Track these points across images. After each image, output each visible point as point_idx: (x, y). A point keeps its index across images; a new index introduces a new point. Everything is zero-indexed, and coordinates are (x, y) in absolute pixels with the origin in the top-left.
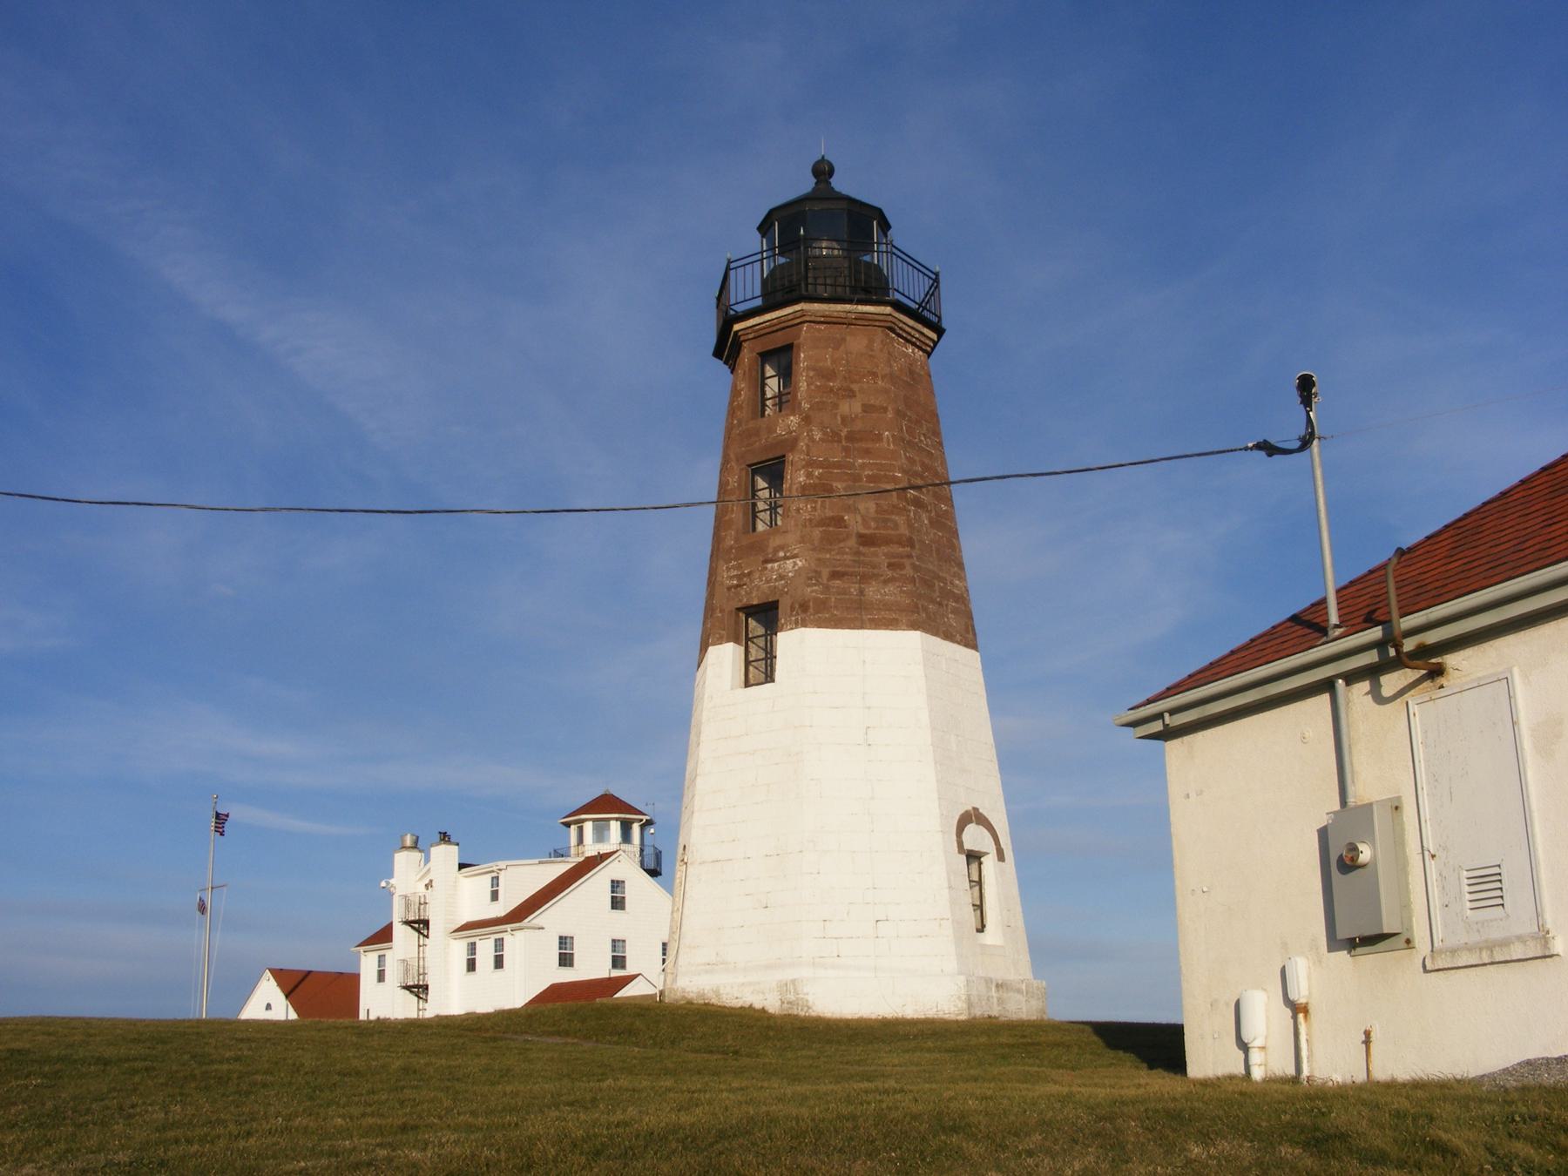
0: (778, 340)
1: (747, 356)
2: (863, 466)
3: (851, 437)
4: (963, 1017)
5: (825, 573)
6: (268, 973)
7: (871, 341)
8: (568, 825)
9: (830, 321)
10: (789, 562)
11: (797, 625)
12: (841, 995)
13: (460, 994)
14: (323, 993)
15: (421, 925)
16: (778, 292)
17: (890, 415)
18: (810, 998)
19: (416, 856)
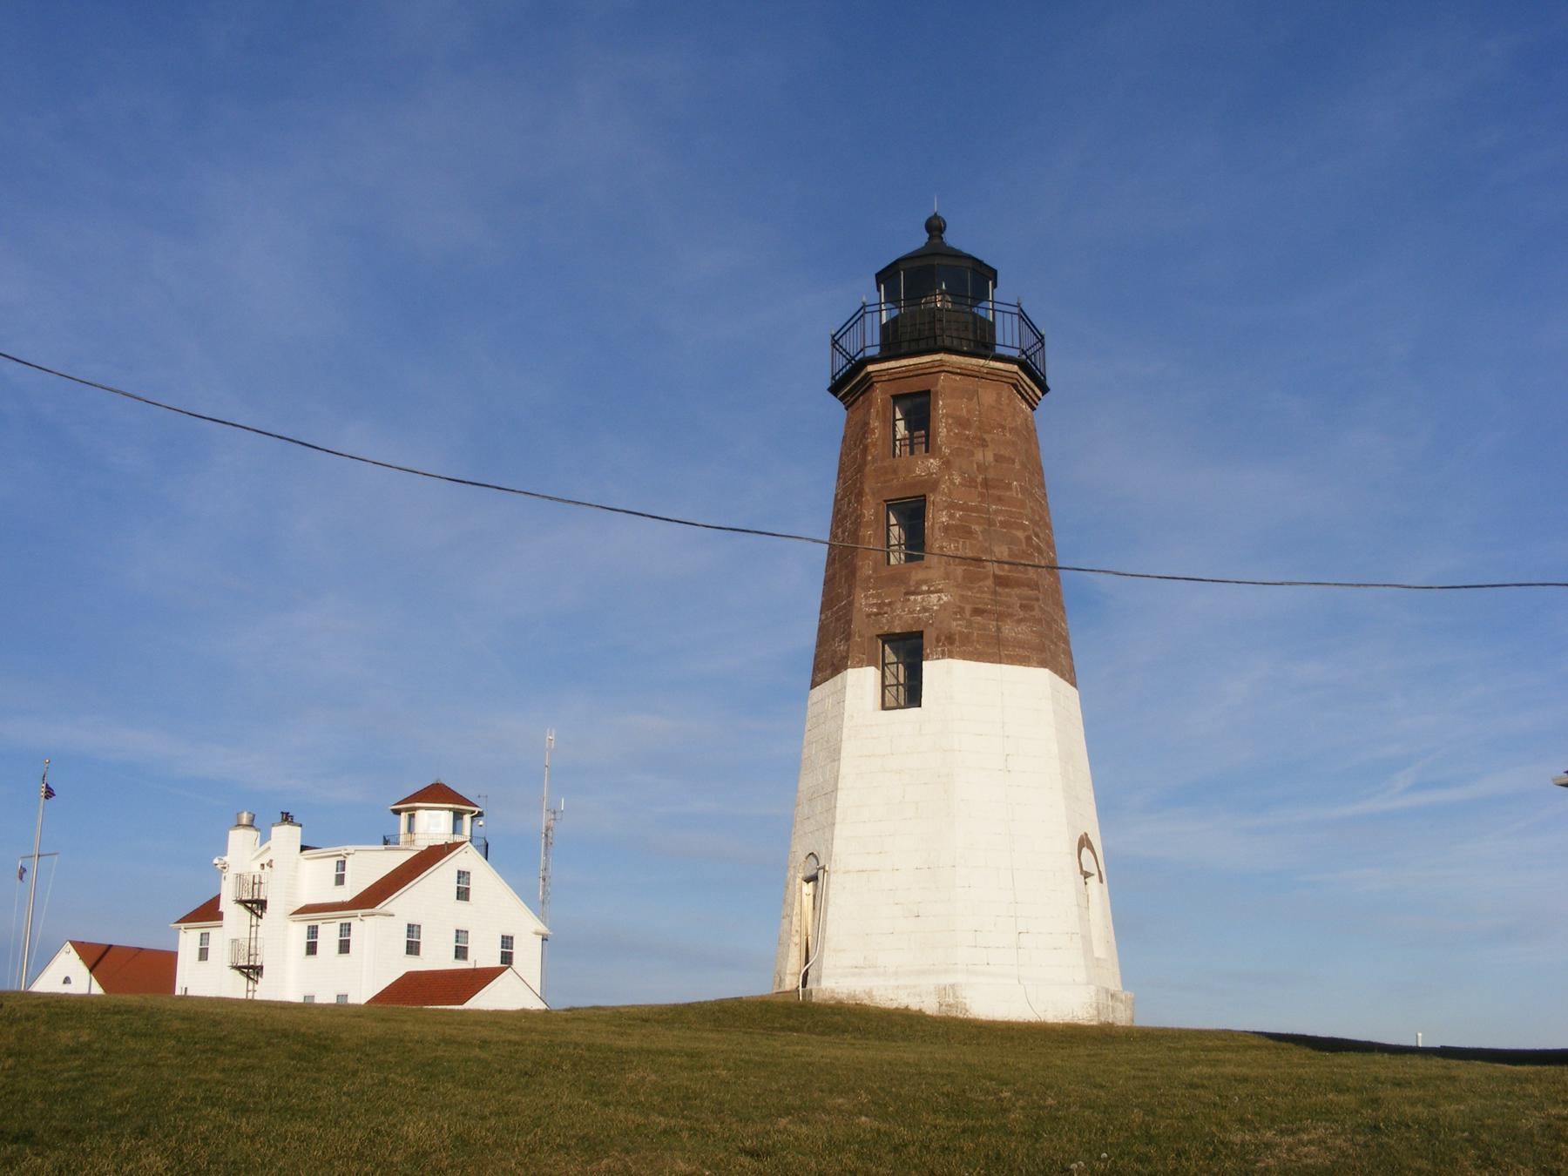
0: (915, 385)
1: (879, 395)
2: (997, 512)
3: (986, 484)
4: (1094, 1023)
5: (968, 608)
6: (69, 946)
7: (999, 395)
8: (397, 812)
9: (965, 373)
10: (934, 597)
11: (943, 655)
12: (993, 1001)
13: (297, 977)
14: (135, 970)
15: (257, 906)
16: (894, 342)
17: (1017, 466)
18: (968, 1001)
19: (252, 835)
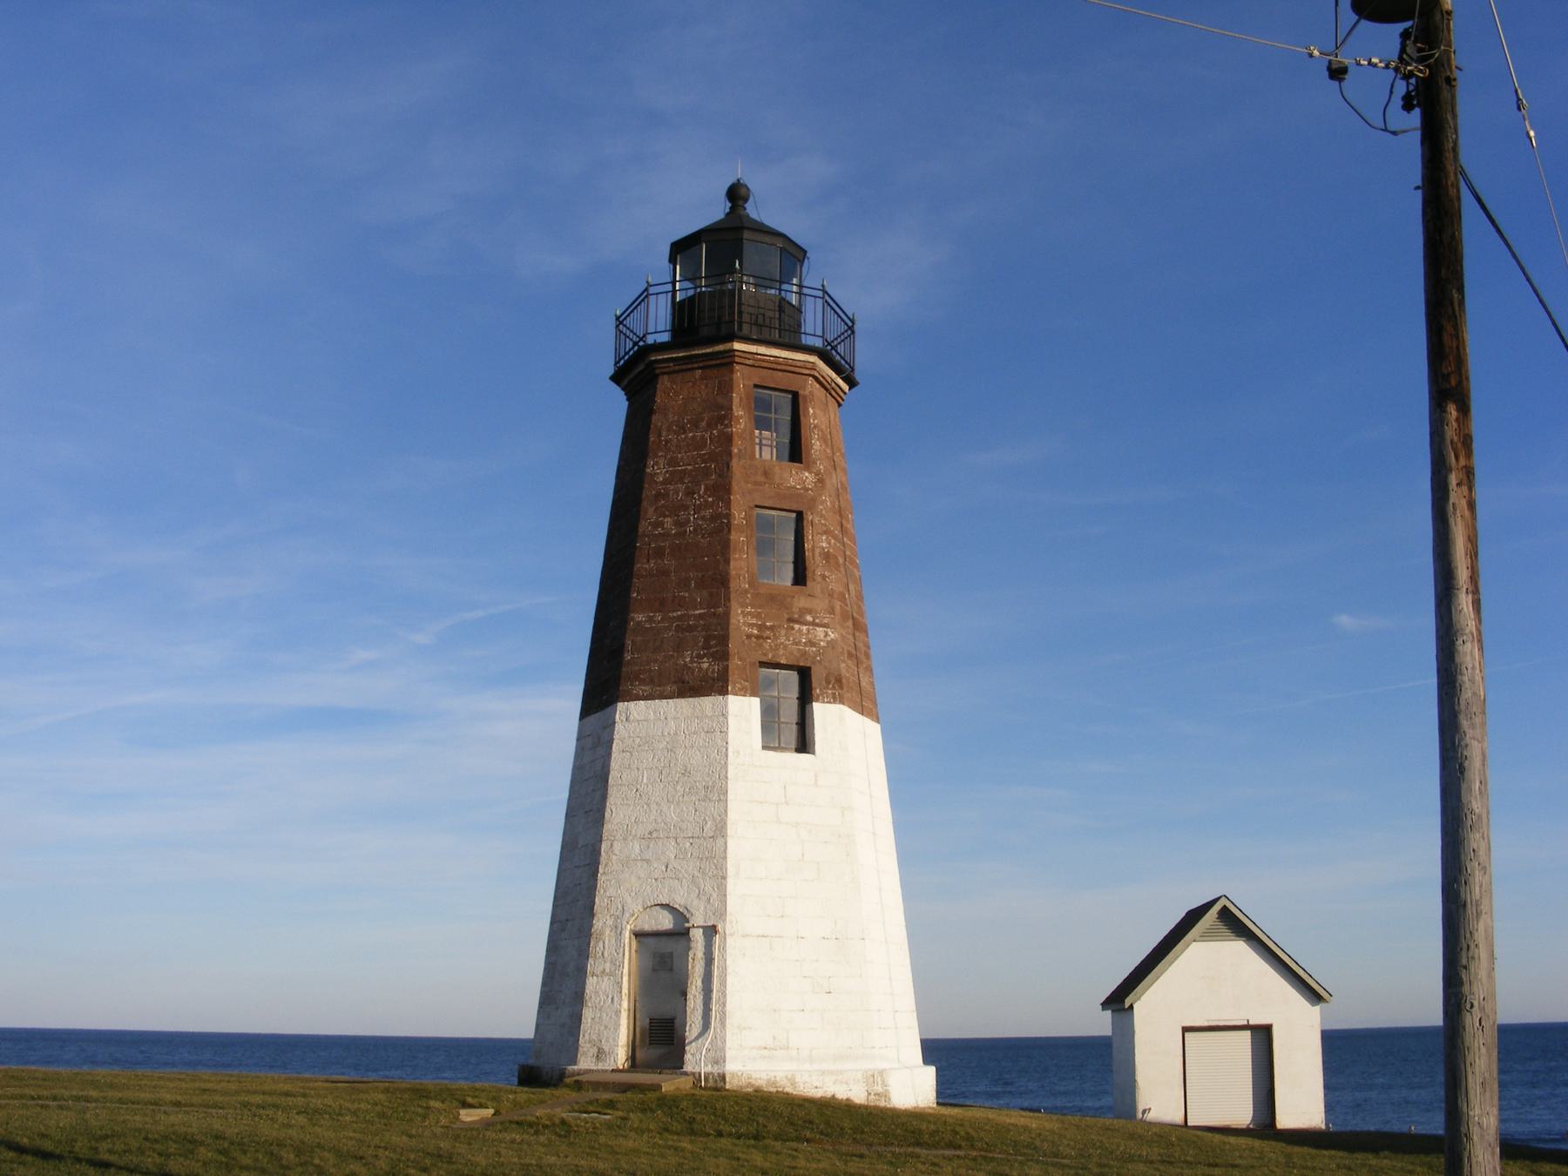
10: (820, 631)
